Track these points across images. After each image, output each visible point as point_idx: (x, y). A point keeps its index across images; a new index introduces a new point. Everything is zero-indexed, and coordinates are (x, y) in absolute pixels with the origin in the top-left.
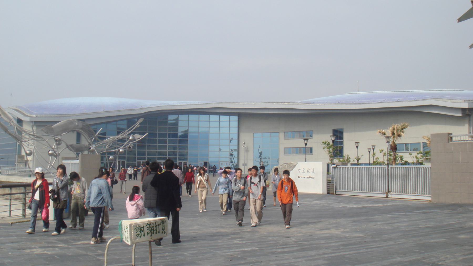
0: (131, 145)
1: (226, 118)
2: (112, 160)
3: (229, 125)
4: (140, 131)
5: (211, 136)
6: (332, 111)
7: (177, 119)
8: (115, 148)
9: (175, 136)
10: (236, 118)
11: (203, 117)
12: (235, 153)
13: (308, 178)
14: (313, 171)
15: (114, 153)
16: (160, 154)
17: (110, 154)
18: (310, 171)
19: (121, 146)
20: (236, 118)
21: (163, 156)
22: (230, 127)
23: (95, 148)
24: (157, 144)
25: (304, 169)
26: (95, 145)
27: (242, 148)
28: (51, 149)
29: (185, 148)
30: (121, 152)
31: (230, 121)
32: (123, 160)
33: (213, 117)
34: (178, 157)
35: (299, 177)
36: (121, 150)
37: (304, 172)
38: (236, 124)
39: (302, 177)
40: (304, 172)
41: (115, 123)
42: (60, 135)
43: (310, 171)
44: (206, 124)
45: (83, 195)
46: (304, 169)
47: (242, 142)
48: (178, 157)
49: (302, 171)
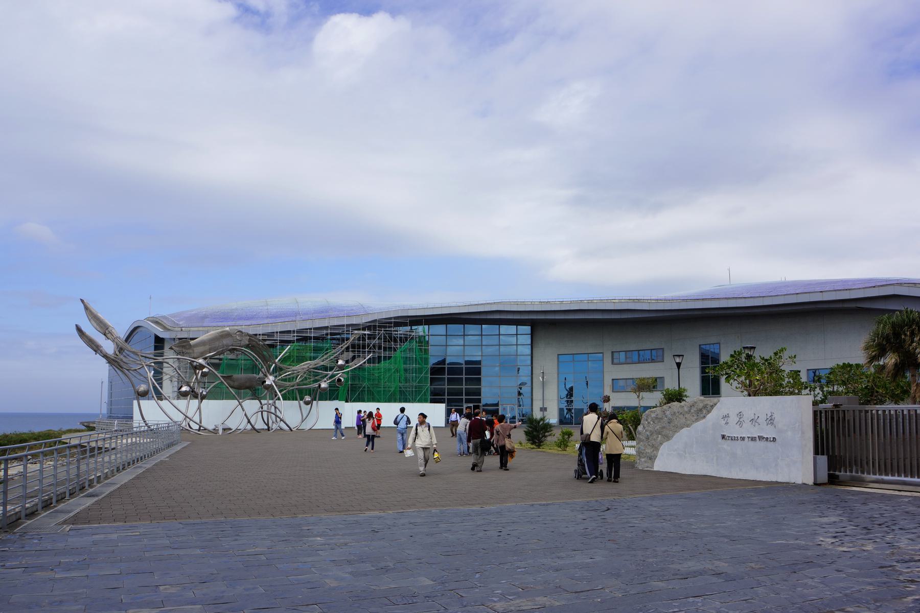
1: (512, 329)
3: (518, 339)
6: (676, 314)
10: (527, 329)
12: (526, 390)
13: (753, 439)
14: (771, 421)
18: (762, 420)
20: (527, 329)
24: (446, 376)
25: (740, 414)
26: (276, 377)
27: (538, 379)
29: (479, 381)
30: (324, 389)
35: (723, 437)
36: (323, 385)
38: (527, 340)
39: (733, 439)
40: (740, 423)
43: (762, 420)
44: (495, 340)
46: (740, 414)
48: (464, 397)
49: (734, 419)
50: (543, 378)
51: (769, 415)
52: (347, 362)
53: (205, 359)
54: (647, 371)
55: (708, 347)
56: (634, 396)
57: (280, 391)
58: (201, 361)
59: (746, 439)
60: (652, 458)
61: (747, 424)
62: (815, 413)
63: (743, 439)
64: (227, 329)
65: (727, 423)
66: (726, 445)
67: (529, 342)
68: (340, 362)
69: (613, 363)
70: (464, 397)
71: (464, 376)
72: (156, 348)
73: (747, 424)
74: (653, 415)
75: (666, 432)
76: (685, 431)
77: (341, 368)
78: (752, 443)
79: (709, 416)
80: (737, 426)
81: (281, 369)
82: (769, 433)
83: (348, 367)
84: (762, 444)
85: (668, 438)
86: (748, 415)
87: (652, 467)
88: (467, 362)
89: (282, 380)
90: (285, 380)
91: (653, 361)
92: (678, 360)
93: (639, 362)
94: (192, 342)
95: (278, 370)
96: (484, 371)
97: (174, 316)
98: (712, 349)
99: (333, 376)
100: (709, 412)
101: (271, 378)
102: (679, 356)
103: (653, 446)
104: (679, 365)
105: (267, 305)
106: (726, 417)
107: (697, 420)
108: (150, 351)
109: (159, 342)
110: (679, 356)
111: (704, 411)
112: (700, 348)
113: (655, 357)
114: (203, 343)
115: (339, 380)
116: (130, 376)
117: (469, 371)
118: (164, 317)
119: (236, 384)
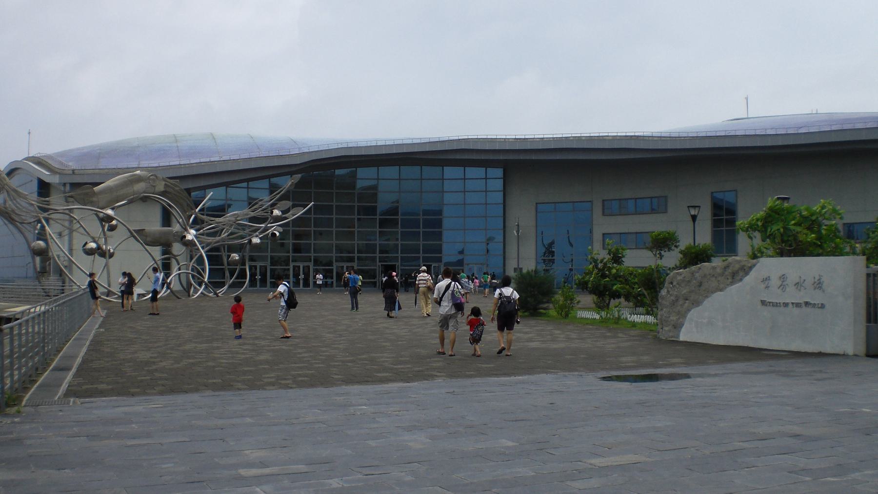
0: (275, 229)
1: (479, 172)
2: (235, 263)
4: (296, 196)
5: (446, 211)
7: (354, 175)
8: (242, 237)
9: (372, 210)
10: (499, 172)
11: (428, 171)
13: (798, 305)
14: (818, 285)
15: (239, 249)
16: (340, 250)
17: (231, 249)
19: (255, 231)
20: (499, 172)
21: (349, 253)
22: (486, 191)
23: (196, 236)
24: (400, 230)
25: (783, 278)
26: (197, 230)
28: (89, 239)
29: (439, 236)
31: (486, 179)
32: (306, 264)
33: (450, 172)
34: (421, 255)
35: (763, 303)
36: (256, 240)
37: (782, 287)
38: (499, 184)
40: (782, 287)
41: (245, 184)
42: (110, 204)
45: (790, 305)
46: (783, 278)
47: (512, 223)
49: (775, 282)
50: (518, 232)
51: (402, 297)
52: (284, 212)
53: (113, 209)
54: (656, 225)
55: (720, 196)
56: (649, 254)
57: (203, 248)
58: (110, 212)
59: (790, 305)
60: (677, 327)
61: (791, 289)
62: (868, 275)
63: (786, 305)
64: (138, 172)
65: (767, 287)
66: (766, 312)
67: (502, 188)
68: (276, 212)
69: (604, 214)
70: (421, 255)
71: (421, 230)
72: (40, 194)
73: (791, 289)
74: (679, 278)
75: (696, 296)
76: (718, 295)
77: (277, 219)
78: (796, 311)
79: (747, 279)
80: (779, 291)
81: (203, 222)
82: (817, 298)
83: (286, 218)
84: (809, 310)
85: (697, 303)
86: (793, 277)
87: (678, 336)
88: (426, 212)
89: (202, 234)
90: (209, 235)
91: (653, 211)
92: (693, 212)
93: (636, 213)
94: (96, 189)
95: (197, 223)
96: (446, 223)
97: (62, 154)
98: (729, 197)
99: (266, 229)
100: (747, 274)
101: (193, 232)
102: (694, 207)
103: (679, 313)
104: (694, 218)
105: (176, 141)
106: (768, 279)
107: (732, 283)
108: (34, 197)
109: (44, 188)
110: (694, 207)
111: (741, 273)
112: (713, 198)
113: (658, 207)
114: (110, 190)
115: (274, 235)
116: (24, 230)
117: (428, 224)
118: (50, 157)
119: (149, 239)
